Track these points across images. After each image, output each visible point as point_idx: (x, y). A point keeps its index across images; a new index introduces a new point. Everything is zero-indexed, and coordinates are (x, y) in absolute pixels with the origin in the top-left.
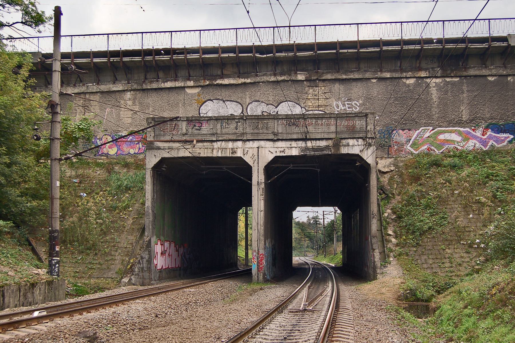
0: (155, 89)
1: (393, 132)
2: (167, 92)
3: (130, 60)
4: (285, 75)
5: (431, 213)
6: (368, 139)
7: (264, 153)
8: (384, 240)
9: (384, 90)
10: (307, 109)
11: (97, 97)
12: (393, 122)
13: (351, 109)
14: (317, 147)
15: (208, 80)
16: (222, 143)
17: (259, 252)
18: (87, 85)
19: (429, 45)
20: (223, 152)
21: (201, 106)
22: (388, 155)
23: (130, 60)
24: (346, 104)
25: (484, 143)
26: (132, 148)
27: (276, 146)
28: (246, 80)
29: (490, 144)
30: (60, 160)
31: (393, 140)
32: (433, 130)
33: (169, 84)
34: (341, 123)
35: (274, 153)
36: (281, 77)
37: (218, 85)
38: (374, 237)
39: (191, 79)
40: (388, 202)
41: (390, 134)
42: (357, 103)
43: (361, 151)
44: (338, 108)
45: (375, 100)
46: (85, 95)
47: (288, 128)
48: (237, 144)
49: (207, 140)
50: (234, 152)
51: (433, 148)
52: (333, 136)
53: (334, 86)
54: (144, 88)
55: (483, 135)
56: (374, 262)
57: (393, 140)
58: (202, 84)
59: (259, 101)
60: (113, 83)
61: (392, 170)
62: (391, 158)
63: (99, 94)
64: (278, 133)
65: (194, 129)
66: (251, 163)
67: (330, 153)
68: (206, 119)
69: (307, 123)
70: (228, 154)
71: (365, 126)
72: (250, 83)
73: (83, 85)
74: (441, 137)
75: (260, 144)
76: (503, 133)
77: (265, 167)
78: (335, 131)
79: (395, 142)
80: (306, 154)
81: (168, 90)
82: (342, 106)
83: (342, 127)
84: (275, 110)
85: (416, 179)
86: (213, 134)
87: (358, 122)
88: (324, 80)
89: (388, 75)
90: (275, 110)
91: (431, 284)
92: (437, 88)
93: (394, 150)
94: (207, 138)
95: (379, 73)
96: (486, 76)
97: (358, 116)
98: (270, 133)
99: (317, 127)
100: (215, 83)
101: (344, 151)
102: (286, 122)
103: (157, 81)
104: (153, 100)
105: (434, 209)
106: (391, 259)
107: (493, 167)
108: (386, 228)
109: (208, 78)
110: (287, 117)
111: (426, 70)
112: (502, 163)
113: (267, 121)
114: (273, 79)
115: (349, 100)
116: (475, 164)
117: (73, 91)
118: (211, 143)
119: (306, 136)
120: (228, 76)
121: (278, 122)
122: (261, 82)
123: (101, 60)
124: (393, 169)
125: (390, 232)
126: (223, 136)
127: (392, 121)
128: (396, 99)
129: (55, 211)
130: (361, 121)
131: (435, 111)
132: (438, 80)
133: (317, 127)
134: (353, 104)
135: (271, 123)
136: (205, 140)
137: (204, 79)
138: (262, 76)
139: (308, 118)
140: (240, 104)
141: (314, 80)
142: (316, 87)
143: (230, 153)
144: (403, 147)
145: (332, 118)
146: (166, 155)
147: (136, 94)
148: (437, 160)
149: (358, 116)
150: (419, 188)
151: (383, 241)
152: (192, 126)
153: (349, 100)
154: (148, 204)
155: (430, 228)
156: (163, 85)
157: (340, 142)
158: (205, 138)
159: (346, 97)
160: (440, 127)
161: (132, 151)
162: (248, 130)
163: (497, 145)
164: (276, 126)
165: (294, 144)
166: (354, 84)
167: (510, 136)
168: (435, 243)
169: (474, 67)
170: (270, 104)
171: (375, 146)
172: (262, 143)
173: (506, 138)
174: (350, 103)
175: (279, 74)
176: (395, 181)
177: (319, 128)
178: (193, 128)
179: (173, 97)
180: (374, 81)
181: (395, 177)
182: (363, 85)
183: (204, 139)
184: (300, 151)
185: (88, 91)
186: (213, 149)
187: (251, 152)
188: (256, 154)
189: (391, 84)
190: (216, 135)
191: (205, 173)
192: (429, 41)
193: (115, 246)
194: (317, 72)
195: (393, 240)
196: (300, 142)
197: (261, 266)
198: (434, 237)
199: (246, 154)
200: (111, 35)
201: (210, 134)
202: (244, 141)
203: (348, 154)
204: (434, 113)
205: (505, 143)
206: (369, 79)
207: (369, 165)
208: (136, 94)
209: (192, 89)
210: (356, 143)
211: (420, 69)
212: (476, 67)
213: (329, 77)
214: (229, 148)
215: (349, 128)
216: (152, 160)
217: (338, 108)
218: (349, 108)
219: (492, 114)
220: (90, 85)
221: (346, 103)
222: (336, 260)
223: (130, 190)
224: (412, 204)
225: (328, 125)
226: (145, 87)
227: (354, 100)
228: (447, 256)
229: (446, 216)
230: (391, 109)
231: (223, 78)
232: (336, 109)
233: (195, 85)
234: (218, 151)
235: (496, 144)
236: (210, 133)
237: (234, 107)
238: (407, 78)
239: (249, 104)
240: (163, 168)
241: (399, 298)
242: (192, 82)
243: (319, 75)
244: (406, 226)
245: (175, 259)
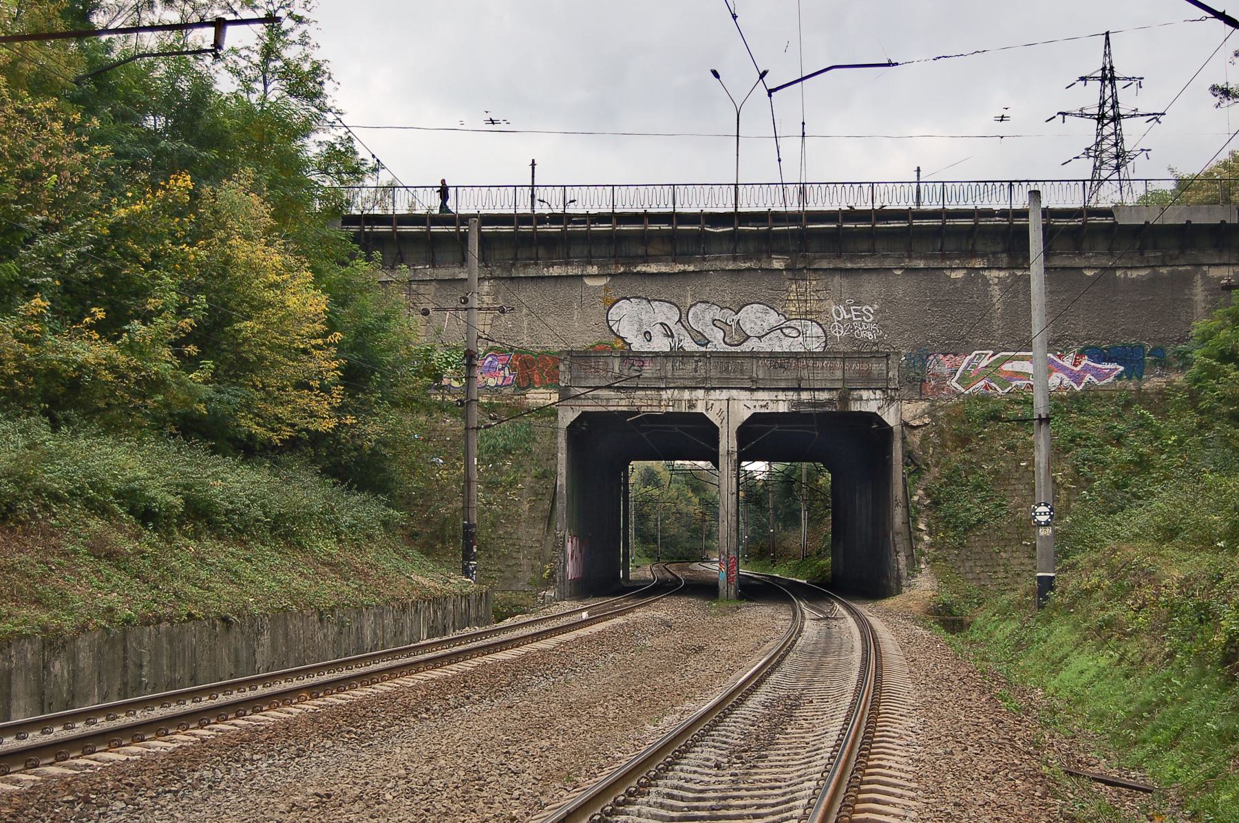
0: (533, 278)
2: (553, 282)
4: (750, 259)
5: (983, 497)
8: (912, 538)
10: (787, 316)
11: (432, 288)
13: (860, 319)
15: (622, 265)
19: (989, 219)
21: (610, 308)
25: (1077, 378)
26: (492, 376)
29: (1086, 379)
30: (478, 428)
32: (993, 355)
33: (556, 271)
35: (752, 408)
36: (745, 262)
37: (639, 273)
38: (898, 534)
40: (919, 478)
41: (924, 361)
42: (870, 308)
43: (879, 408)
44: (839, 317)
50: (692, 406)
51: (993, 385)
52: (839, 385)
53: (832, 280)
54: (513, 275)
55: (1075, 365)
56: (898, 570)
59: (708, 303)
62: (925, 400)
63: (434, 283)
64: (758, 379)
66: (717, 423)
69: (800, 365)
70: (684, 409)
71: (885, 372)
74: (1007, 367)
76: (1108, 362)
78: (841, 377)
82: (845, 313)
84: (735, 318)
85: (963, 440)
87: (875, 365)
89: (921, 264)
90: (735, 318)
91: (975, 601)
92: (1000, 287)
95: (907, 260)
96: (1081, 268)
100: (635, 271)
101: (855, 407)
103: (536, 264)
104: (528, 297)
105: (988, 491)
106: (923, 566)
107: (1084, 422)
108: (915, 520)
110: (773, 356)
111: (983, 256)
112: (1099, 416)
114: (731, 266)
116: (1056, 418)
119: (799, 385)
120: (656, 259)
125: (922, 526)
128: (934, 304)
129: (472, 498)
131: (997, 323)
132: (1002, 274)
134: (863, 310)
135: (747, 364)
137: (616, 264)
138: (713, 260)
140: (676, 306)
141: (800, 270)
142: (803, 280)
144: (945, 383)
147: (498, 284)
148: (996, 411)
150: (967, 456)
151: (911, 539)
154: (562, 480)
155: (979, 521)
156: (545, 272)
157: (849, 394)
160: (1006, 350)
161: (492, 382)
162: (713, 374)
163: (1097, 382)
164: (755, 369)
165: (781, 395)
166: (865, 276)
167: (1118, 367)
168: (985, 544)
169: (1061, 254)
170: (726, 308)
172: (734, 393)
173: (1112, 370)
174: (859, 308)
176: (930, 442)
179: (562, 291)
180: (899, 272)
187: (717, 406)
192: (989, 213)
193: (514, 545)
194: (804, 257)
195: (926, 538)
196: (791, 393)
197: (732, 575)
198: (985, 534)
200: (462, 188)
201: (655, 378)
202: (708, 390)
203: (861, 412)
204: (995, 327)
205: (1110, 380)
206: (890, 269)
207: (892, 428)
208: (498, 284)
210: (872, 396)
211: (973, 254)
212: (1064, 253)
213: (824, 264)
216: (568, 416)
217: (839, 317)
218: (856, 316)
219: (1089, 331)
220: (419, 267)
222: (809, 571)
223: (510, 453)
224: (955, 482)
227: (865, 304)
228: (1001, 562)
229: (1004, 503)
232: (835, 317)
235: (1095, 380)
236: (655, 375)
237: (666, 310)
238: (952, 269)
239: (691, 306)
241: (928, 612)
244: (945, 517)
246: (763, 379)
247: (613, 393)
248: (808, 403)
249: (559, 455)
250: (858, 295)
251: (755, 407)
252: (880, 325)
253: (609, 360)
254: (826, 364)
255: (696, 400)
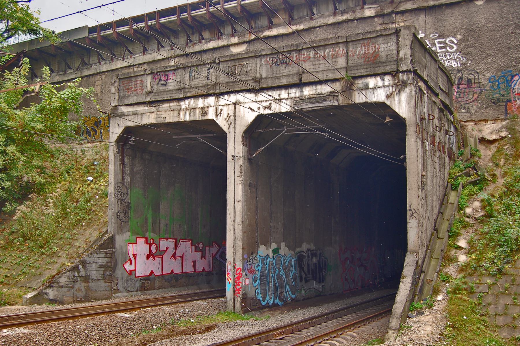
1: (514, 79)
6: (401, 74)
9: (497, 15)
11: (171, 73)
12: (513, 63)
13: (444, 50)
17: (236, 265)
18: (135, 56)
20: (192, 114)
22: (506, 115)
24: (436, 43)
27: (258, 100)
28: (298, 26)
31: (514, 91)
34: (355, 51)
43: (388, 97)
45: (482, 31)
46: (134, 68)
47: (274, 69)
53: (418, 19)
57: (514, 91)
58: (247, 40)
61: (502, 137)
64: (261, 78)
65: (159, 85)
66: (225, 128)
67: (336, 104)
69: (302, 57)
70: (198, 117)
71: (395, 52)
72: (304, 30)
75: (238, 98)
77: (245, 132)
79: (517, 94)
80: (302, 109)
81: (212, 52)
83: (356, 57)
86: (180, 89)
87: (382, 46)
88: (403, 12)
93: (517, 106)
94: (174, 95)
97: (382, 36)
99: (317, 63)
100: (262, 36)
101: (359, 98)
102: (272, 61)
113: (246, 61)
115: (441, 36)
117: (122, 64)
118: (179, 102)
119: (301, 80)
120: (278, 25)
121: (261, 61)
122: (317, 27)
124: (504, 136)
125: (462, 243)
127: (512, 61)
130: (387, 43)
133: (317, 63)
134: (447, 41)
136: (171, 98)
139: (303, 49)
141: (389, 14)
145: (341, 45)
146: (130, 124)
149: (382, 36)
152: (157, 80)
153: (441, 36)
159: (436, 33)
164: (258, 69)
165: (284, 94)
166: (448, 11)
171: (412, 86)
172: (239, 97)
177: (319, 64)
178: (158, 84)
181: (505, 148)
182: (461, 11)
184: (293, 104)
186: (180, 111)
188: (231, 114)
189: (508, 5)
197: (238, 287)
199: (219, 115)
207: (404, 119)
210: (380, 83)
214: (199, 107)
215: (369, 58)
221: (436, 41)
225: (334, 57)
227: (448, 36)
230: (509, 42)
231: (271, 28)
242: (236, 38)
243: (394, 5)
245: (194, 262)
246: (266, 78)
247: (146, 108)
248: (310, 98)
249: (110, 166)
250: (441, 29)
251: (259, 108)
252: (464, 53)
253: (144, 78)
254: (328, 53)
255: (208, 107)
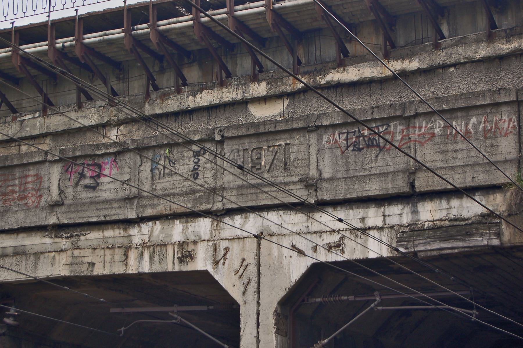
3: (102, 38)
7: (276, 254)
11: (108, 160)
14: (451, 220)
16: (155, 227)
20: (156, 259)
23: (102, 38)
28: (406, 62)
36: (509, 42)
39: (260, 79)
46: (20, 145)
47: (351, 160)
48: (197, 229)
49: (113, 218)
60: (76, 108)
64: (321, 179)
65: (79, 188)
66: (235, 294)
67: (496, 242)
68: (111, 150)
69: (415, 134)
72: (419, 72)
73: (12, 121)
81: (205, 114)
86: (128, 199)
94: (114, 212)
98: (294, 183)
99: (450, 147)
100: (323, 82)
109: (306, 70)
118: (125, 229)
121: (320, 139)
123: (36, 47)
126: (156, 202)
133: (450, 147)
143: (176, 261)
145: (504, 109)
152: (75, 177)
158: (107, 212)
164: (313, 157)
175: (503, 34)
177: (456, 151)
178: (77, 184)
183: (105, 216)
185: (24, 135)
186: (127, 249)
188: (251, 260)
190: (136, 202)
191: (124, 330)
199: (222, 261)
201: (120, 200)
209: (267, 105)
214: (173, 242)
225: (489, 134)
226: (148, 110)
233: (272, 92)
234: (142, 254)
236: (121, 194)
240: (9, 316)
242: (264, 84)
247: (48, 240)
254: (476, 126)
255: (195, 243)
